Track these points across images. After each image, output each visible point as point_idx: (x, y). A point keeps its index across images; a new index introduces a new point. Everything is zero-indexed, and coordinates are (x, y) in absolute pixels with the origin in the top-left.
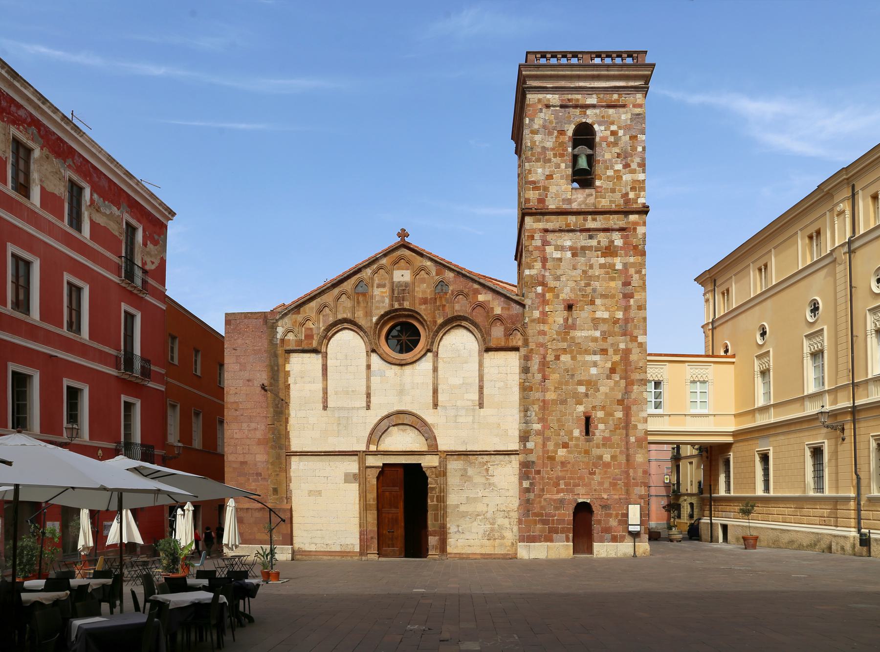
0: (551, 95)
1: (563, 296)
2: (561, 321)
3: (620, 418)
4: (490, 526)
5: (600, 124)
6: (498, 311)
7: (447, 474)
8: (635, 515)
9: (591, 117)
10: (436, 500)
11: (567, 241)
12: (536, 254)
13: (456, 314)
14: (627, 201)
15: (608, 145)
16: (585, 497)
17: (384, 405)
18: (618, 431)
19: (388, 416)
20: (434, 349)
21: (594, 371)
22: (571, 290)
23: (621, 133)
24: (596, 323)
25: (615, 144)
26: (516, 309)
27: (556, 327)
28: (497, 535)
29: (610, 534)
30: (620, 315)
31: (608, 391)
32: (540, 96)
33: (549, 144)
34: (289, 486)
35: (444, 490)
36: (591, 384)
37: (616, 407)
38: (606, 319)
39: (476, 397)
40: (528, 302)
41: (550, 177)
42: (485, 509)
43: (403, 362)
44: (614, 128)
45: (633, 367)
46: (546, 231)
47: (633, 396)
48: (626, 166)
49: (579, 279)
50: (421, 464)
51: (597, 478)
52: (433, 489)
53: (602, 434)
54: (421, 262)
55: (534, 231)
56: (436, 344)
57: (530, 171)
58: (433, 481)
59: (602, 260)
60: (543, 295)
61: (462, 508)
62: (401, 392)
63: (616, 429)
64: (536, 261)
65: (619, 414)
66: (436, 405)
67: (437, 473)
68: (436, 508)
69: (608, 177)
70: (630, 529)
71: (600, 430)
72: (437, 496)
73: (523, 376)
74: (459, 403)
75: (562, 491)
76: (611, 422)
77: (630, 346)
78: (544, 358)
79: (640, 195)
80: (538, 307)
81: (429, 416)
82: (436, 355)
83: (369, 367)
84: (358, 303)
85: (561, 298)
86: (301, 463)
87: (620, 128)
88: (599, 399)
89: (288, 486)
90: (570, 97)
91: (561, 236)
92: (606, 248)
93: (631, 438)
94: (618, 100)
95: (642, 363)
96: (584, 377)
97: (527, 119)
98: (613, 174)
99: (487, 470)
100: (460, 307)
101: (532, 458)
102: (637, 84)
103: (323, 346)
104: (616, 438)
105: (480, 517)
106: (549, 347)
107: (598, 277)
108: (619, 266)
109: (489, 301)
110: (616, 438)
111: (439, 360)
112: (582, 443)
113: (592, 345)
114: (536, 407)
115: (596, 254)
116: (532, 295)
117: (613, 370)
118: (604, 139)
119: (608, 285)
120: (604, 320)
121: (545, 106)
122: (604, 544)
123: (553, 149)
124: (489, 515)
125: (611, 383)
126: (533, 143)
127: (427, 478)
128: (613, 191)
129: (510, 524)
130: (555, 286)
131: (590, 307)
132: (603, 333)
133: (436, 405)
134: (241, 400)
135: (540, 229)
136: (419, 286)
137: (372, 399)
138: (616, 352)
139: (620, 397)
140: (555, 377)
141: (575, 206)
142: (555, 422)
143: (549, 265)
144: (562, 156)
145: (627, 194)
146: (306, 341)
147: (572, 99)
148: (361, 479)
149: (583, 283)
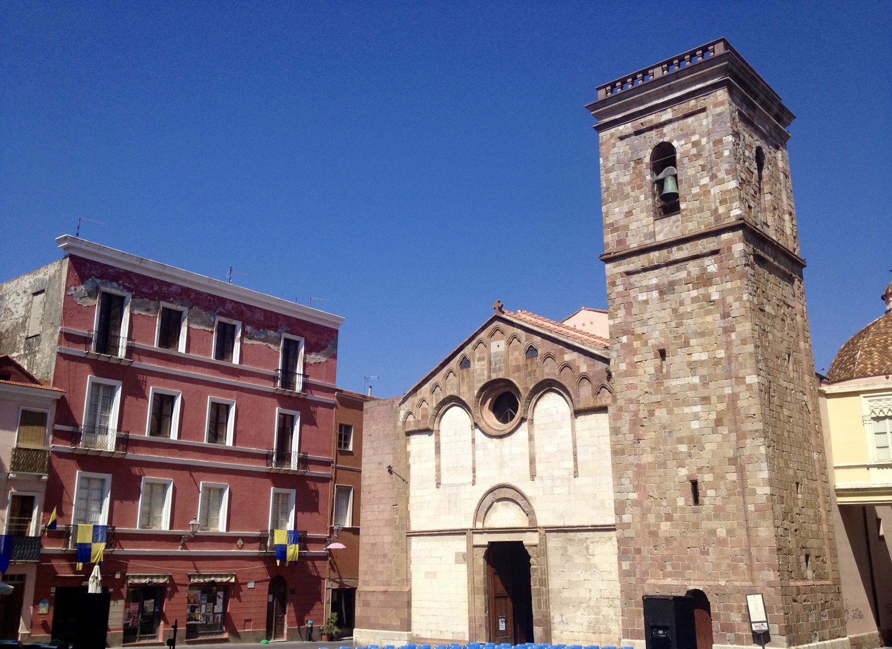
0: (623, 126)
1: (651, 342)
2: (653, 371)
3: (734, 482)
4: (594, 617)
5: (679, 139)
6: (584, 369)
7: (548, 553)
8: (757, 609)
9: (668, 134)
10: (539, 583)
11: (652, 279)
12: (618, 301)
13: (546, 377)
14: (718, 218)
15: (690, 160)
16: (697, 583)
17: (488, 478)
18: (733, 498)
19: (491, 491)
20: (529, 417)
21: (695, 425)
22: (661, 334)
23: (704, 141)
24: (693, 367)
25: (698, 155)
26: (601, 366)
27: (647, 378)
28: (602, 628)
29: (733, 634)
30: (721, 354)
31: (715, 448)
32: (613, 130)
33: (625, 179)
34: (409, 567)
35: (545, 571)
36: (694, 441)
37: (727, 467)
38: (705, 361)
39: (571, 465)
40: (613, 355)
41: (629, 213)
42: (588, 595)
43: (502, 433)
44: (695, 138)
45: (743, 416)
46: (629, 273)
47: (747, 452)
48: (713, 177)
49: (669, 320)
50: (522, 542)
51: (712, 557)
52: (535, 569)
53: (712, 502)
54: (513, 330)
55: (614, 276)
56: (530, 411)
57: (607, 213)
58: (535, 561)
59: (694, 293)
60: (629, 345)
61: (565, 594)
62: (502, 464)
63: (730, 495)
64: (619, 308)
65: (733, 477)
66: (533, 476)
67: (538, 551)
68: (539, 593)
69: (694, 196)
70: (754, 628)
71: (709, 496)
72: (539, 578)
73: (615, 438)
74: (556, 473)
75: (670, 575)
76: (723, 487)
77: (737, 389)
78: (636, 414)
79: (732, 206)
80: (625, 359)
81: (527, 488)
82: (532, 421)
83: (473, 441)
84: (463, 379)
85: (649, 344)
86: (420, 543)
87: (702, 136)
88: (705, 457)
89: (408, 567)
90: (643, 120)
91: (645, 276)
92: (698, 278)
93: (749, 506)
94: (696, 106)
95: (754, 410)
96: (684, 433)
97: (601, 159)
98: (699, 190)
99: (587, 548)
100: (549, 371)
101: (629, 533)
102: (716, 80)
103: (435, 425)
104: (731, 507)
105: (584, 605)
106: (641, 402)
107: (691, 313)
108: (715, 296)
109: (575, 360)
110: (731, 507)
111: (535, 428)
112: (690, 516)
113: (690, 394)
114: (630, 473)
115: (686, 287)
116: (617, 346)
117: (719, 422)
118: (685, 155)
119: (704, 320)
120: (702, 363)
121: (618, 140)
122: (726, 646)
123: (630, 182)
124: (592, 603)
125: (718, 438)
126: (608, 180)
127: (529, 557)
128: (700, 210)
129: (615, 615)
130: (642, 332)
131: (684, 350)
132: (703, 378)
133: (533, 476)
134: (373, 483)
135: (621, 273)
136: (512, 354)
137: (477, 473)
138: (721, 398)
139: (731, 453)
140: (650, 436)
141: (661, 238)
142: (655, 490)
143: (635, 310)
144: (640, 187)
145: (716, 209)
146: (423, 421)
147: (646, 122)
148: (469, 560)
149: (673, 324)
